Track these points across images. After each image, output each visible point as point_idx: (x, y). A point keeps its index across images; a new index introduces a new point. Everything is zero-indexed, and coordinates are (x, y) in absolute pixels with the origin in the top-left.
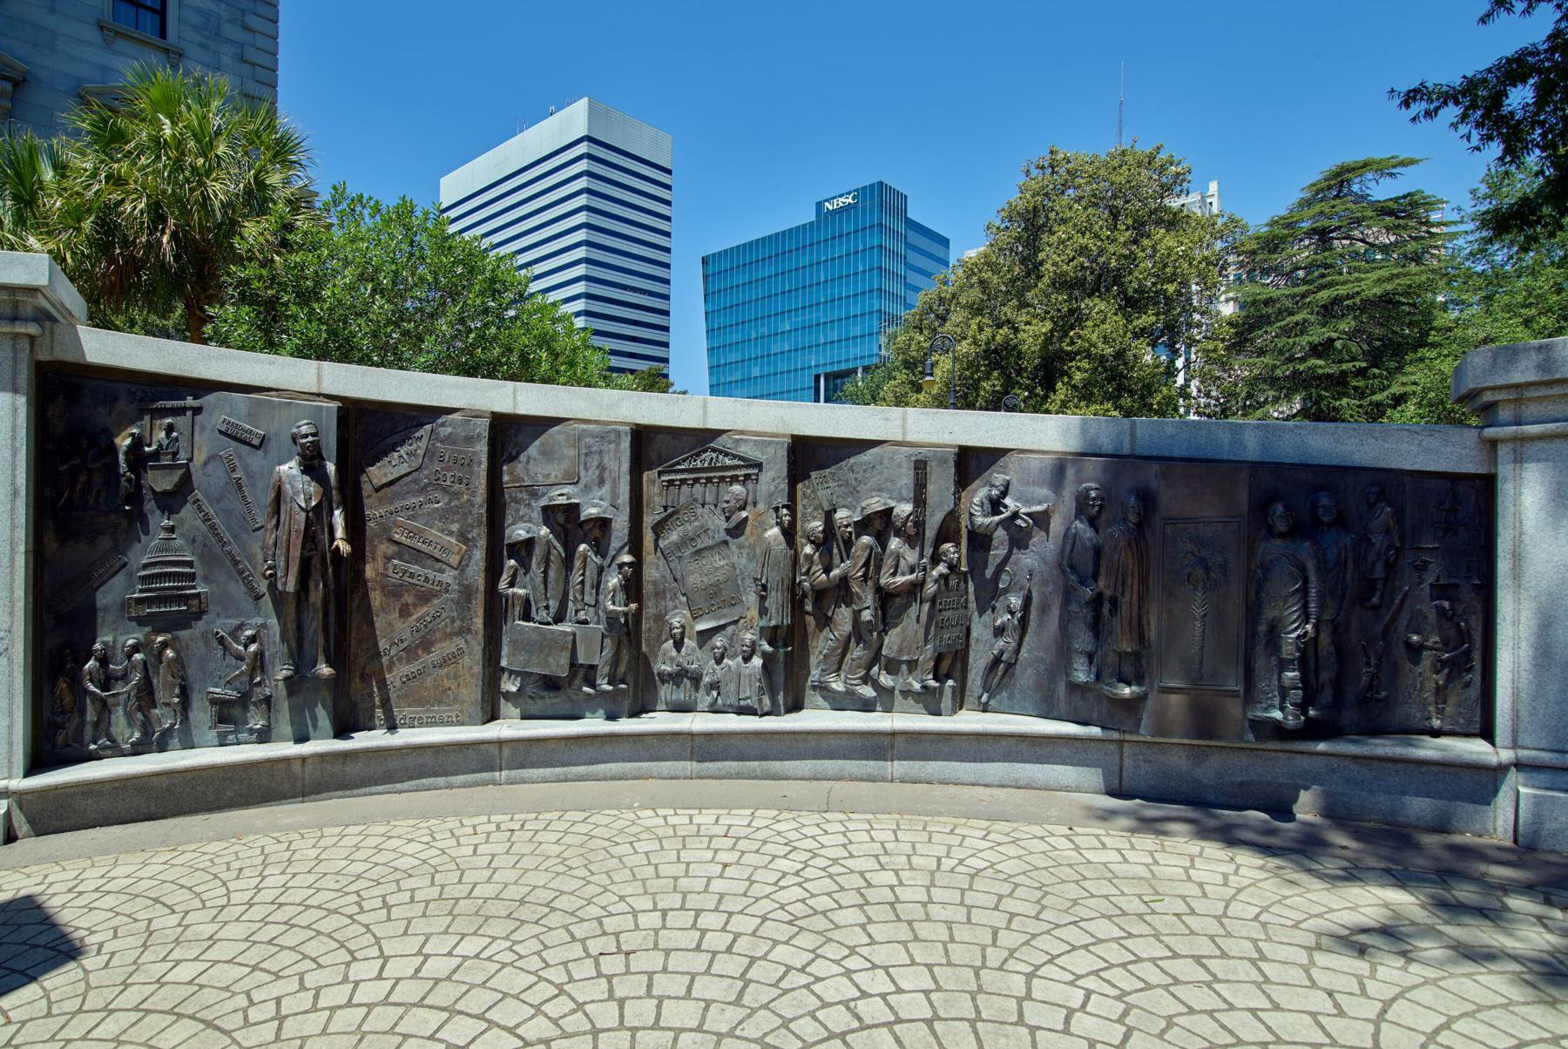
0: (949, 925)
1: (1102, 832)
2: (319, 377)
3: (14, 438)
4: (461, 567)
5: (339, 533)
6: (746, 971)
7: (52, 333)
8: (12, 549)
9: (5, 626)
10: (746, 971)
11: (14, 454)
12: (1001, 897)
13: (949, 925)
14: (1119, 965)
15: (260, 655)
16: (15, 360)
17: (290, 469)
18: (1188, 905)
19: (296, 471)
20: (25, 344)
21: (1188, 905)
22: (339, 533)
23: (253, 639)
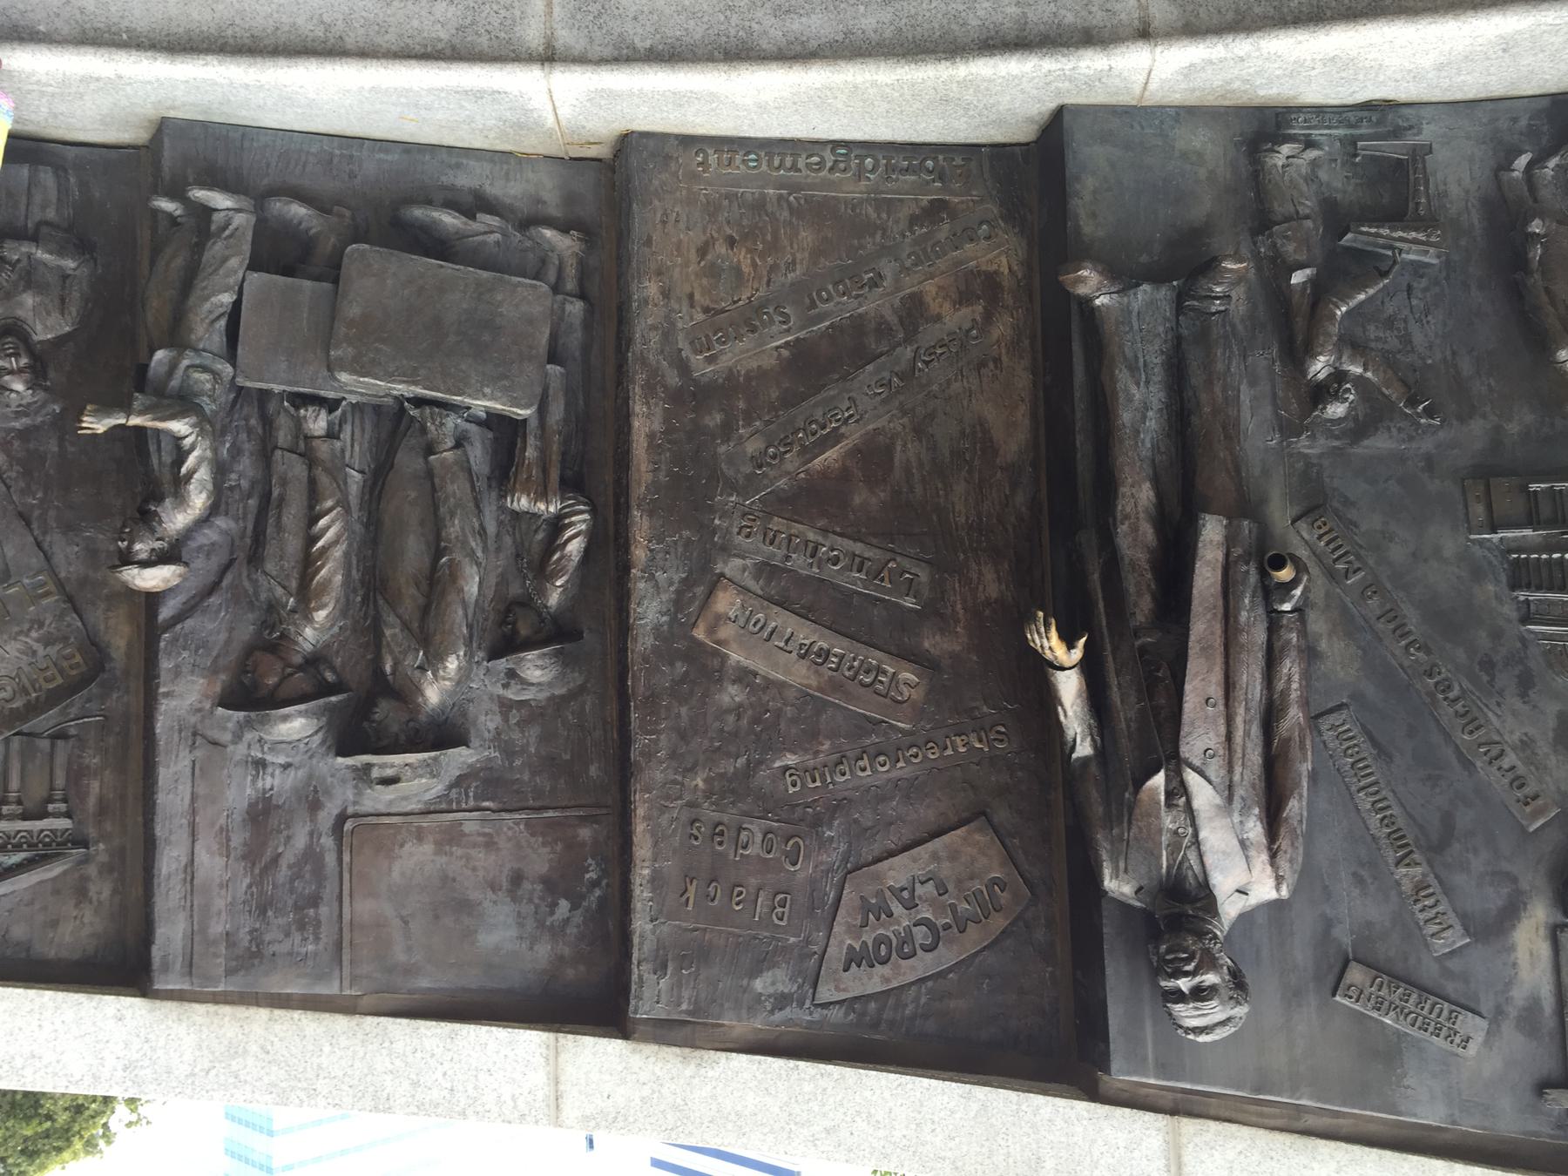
4: (702, 580)
5: (1069, 686)
15: (1296, 353)
17: (1242, 879)
19: (1224, 882)
22: (1069, 686)
23: (1322, 393)
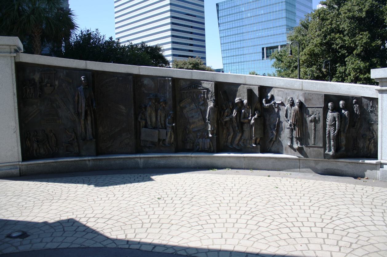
0: (215, 219)
1: (338, 183)
2: (86, 65)
3: (13, 81)
6: (247, 222)
7: (19, 55)
8: (15, 108)
9: (15, 126)
10: (247, 222)
11: (13, 85)
12: (342, 236)
13: (215, 219)
14: (352, 228)
16: (12, 62)
18: (362, 210)
20: (13, 58)
21: (362, 210)
